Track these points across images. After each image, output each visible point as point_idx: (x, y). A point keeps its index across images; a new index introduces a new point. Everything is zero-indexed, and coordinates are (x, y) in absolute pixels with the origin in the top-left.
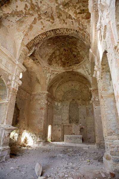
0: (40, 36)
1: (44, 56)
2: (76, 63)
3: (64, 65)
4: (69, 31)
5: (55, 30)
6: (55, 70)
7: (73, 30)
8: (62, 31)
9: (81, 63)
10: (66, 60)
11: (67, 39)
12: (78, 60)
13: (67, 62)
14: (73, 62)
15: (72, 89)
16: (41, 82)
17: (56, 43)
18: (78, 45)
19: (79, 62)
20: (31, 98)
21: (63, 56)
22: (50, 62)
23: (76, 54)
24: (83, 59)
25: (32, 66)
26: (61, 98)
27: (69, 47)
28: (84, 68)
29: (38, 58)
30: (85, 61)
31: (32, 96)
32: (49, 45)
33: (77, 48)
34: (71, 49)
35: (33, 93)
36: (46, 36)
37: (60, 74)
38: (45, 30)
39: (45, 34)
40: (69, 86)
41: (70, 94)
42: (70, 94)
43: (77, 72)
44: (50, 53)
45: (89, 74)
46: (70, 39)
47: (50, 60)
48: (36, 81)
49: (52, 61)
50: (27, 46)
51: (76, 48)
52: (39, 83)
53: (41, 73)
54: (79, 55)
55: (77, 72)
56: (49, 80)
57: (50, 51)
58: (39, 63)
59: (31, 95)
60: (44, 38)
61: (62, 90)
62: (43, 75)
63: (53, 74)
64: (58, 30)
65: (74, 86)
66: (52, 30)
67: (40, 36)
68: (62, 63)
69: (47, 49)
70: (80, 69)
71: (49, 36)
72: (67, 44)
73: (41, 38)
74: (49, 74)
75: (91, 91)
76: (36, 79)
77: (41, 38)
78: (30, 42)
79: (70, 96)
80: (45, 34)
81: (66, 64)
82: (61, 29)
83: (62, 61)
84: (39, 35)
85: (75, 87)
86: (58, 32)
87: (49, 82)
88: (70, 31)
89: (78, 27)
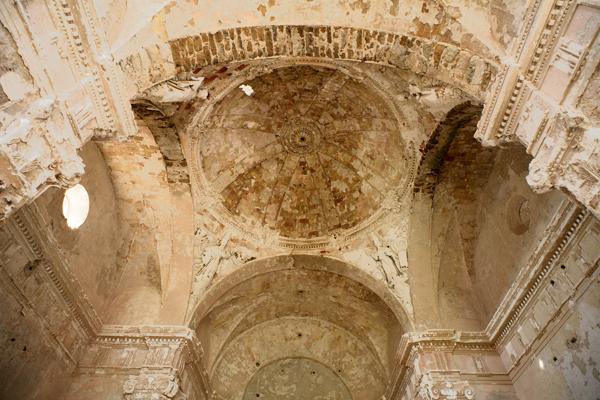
0: (243, 36)
1: (216, 166)
2: (339, 226)
3: (287, 226)
4: (367, 41)
5: (311, 29)
6: (249, 239)
7: (391, 36)
8: (338, 41)
9: (365, 223)
10: (297, 208)
11: (322, 120)
12: (350, 215)
13: (304, 217)
14: (326, 220)
15: (297, 355)
16: (168, 280)
17: (279, 126)
18: (361, 154)
19: (354, 224)
20: (87, 360)
21: (288, 192)
22: (233, 198)
23: (342, 188)
24: (371, 210)
25: (150, 197)
26: (241, 393)
27: (324, 157)
28: (378, 243)
29: (193, 159)
30: (381, 217)
31: (95, 349)
32: (251, 124)
33: (356, 164)
34: (327, 165)
35: (110, 330)
36: (269, 45)
37: (265, 261)
38: (272, 18)
39: (265, 33)
40: (286, 340)
41: (286, 378)
42: (286, 378)
43: (342, 266)
44: (241, 162)
45: (399, 273)
46: (337, 123)
47: (233, 192)
48: (145, 277)
49: (243, 201)
50: (177, 46)
51: (349, 166)
52: (159, 285)
53: (179, 238)
54: (356, 195)
55: (337, 262)
56: (211, 275)
57: (243, 152)
58: (185, 185)
59: (93, 336)
60: (255, 49)
61: (249, 351)
62: (189, 250)
63: (236, 255)
64: (324, 35)
65: (304, 339)
66: (301, 29)
67: (243, 36)
68: (280, 218)
69: (237, 143)
70: (357, 248)
71: (278, 49)
72: (317, 139)
73: (245, 45)
74: (218, 252)
75: (415, 349)
76: (144, 265)
77: (245, 45)
78: (197, 38)
79: (285, 389)
80: (269, 34)
81: (298, 226)
82: (336, 29)
83: (281, 211)
84: (239, 31)
85: (308, 346)
86: (320, 41)
87: (207, 288)
88: (372, 46)
89: (416, 19)
